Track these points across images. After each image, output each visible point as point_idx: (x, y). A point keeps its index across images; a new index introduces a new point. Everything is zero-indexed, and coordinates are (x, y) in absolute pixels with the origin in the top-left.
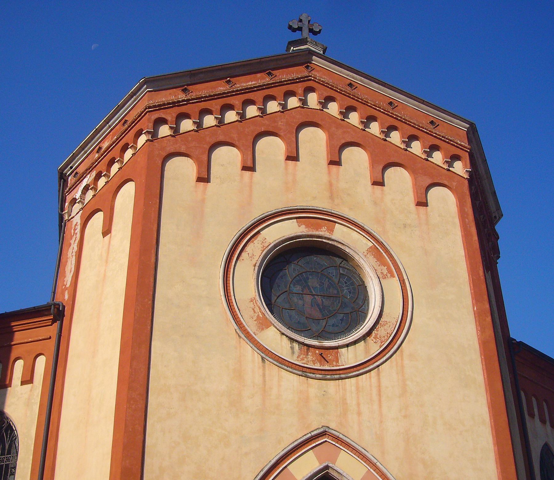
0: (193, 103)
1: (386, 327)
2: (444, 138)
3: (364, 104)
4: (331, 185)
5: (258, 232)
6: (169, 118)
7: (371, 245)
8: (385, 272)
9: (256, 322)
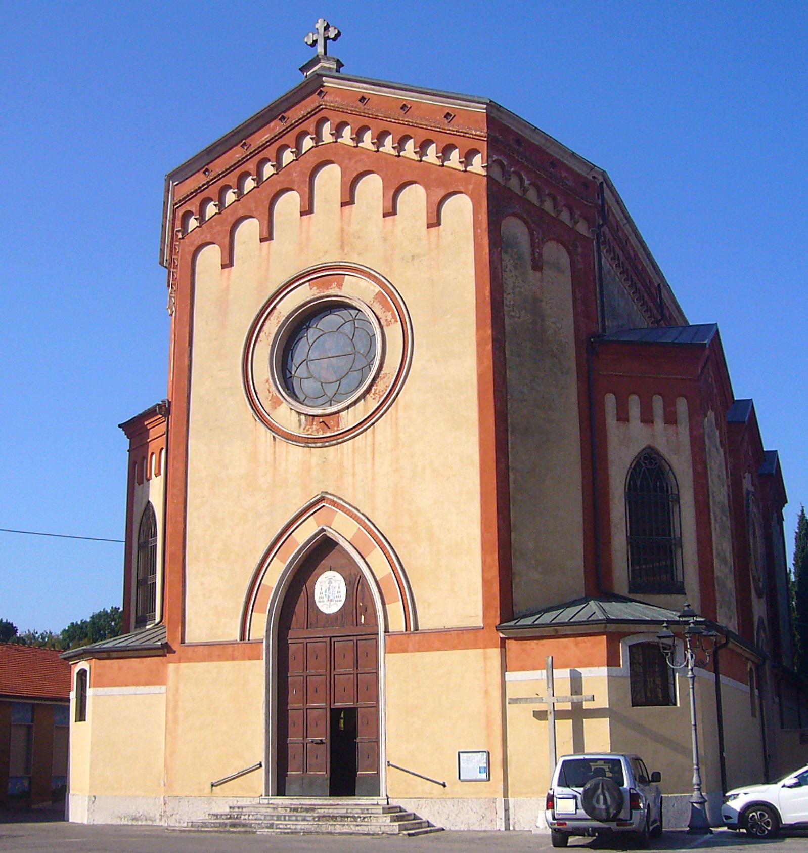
0: (213, 183)
1: (385, 380)
2: (459, 132)
3: (376, 119)
4: (342, 230)
5: (274, 307)
6: (193, 210)
7: (377, 291)
8: (390, 317)
9: (270, 402)
